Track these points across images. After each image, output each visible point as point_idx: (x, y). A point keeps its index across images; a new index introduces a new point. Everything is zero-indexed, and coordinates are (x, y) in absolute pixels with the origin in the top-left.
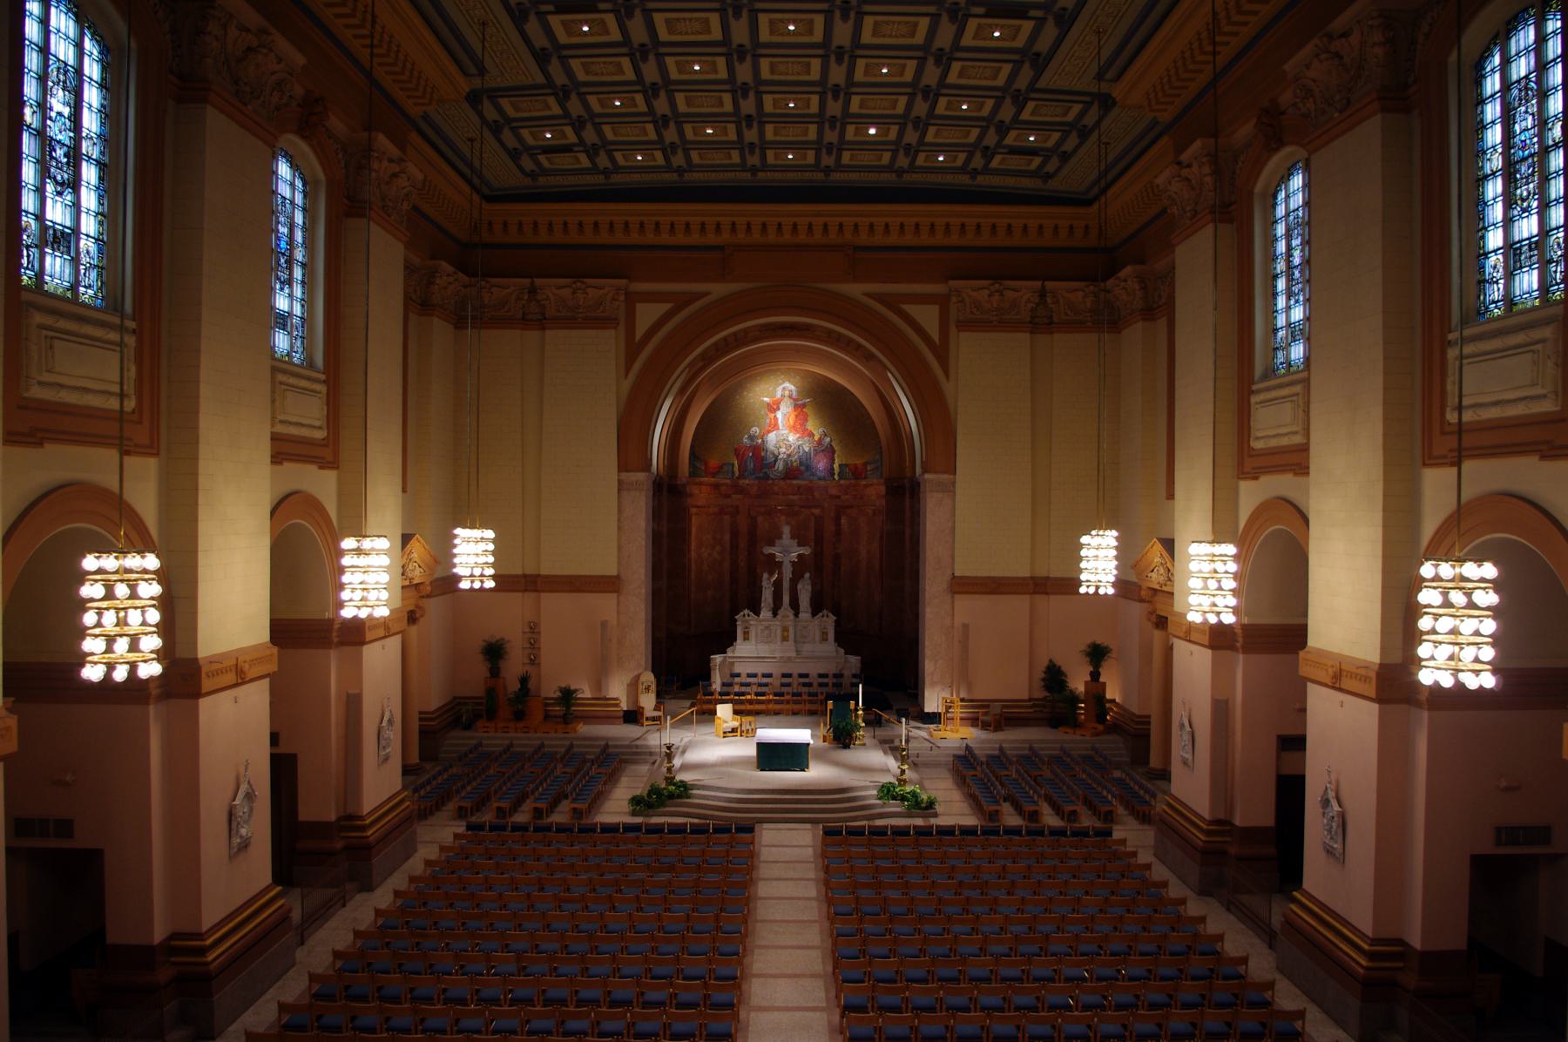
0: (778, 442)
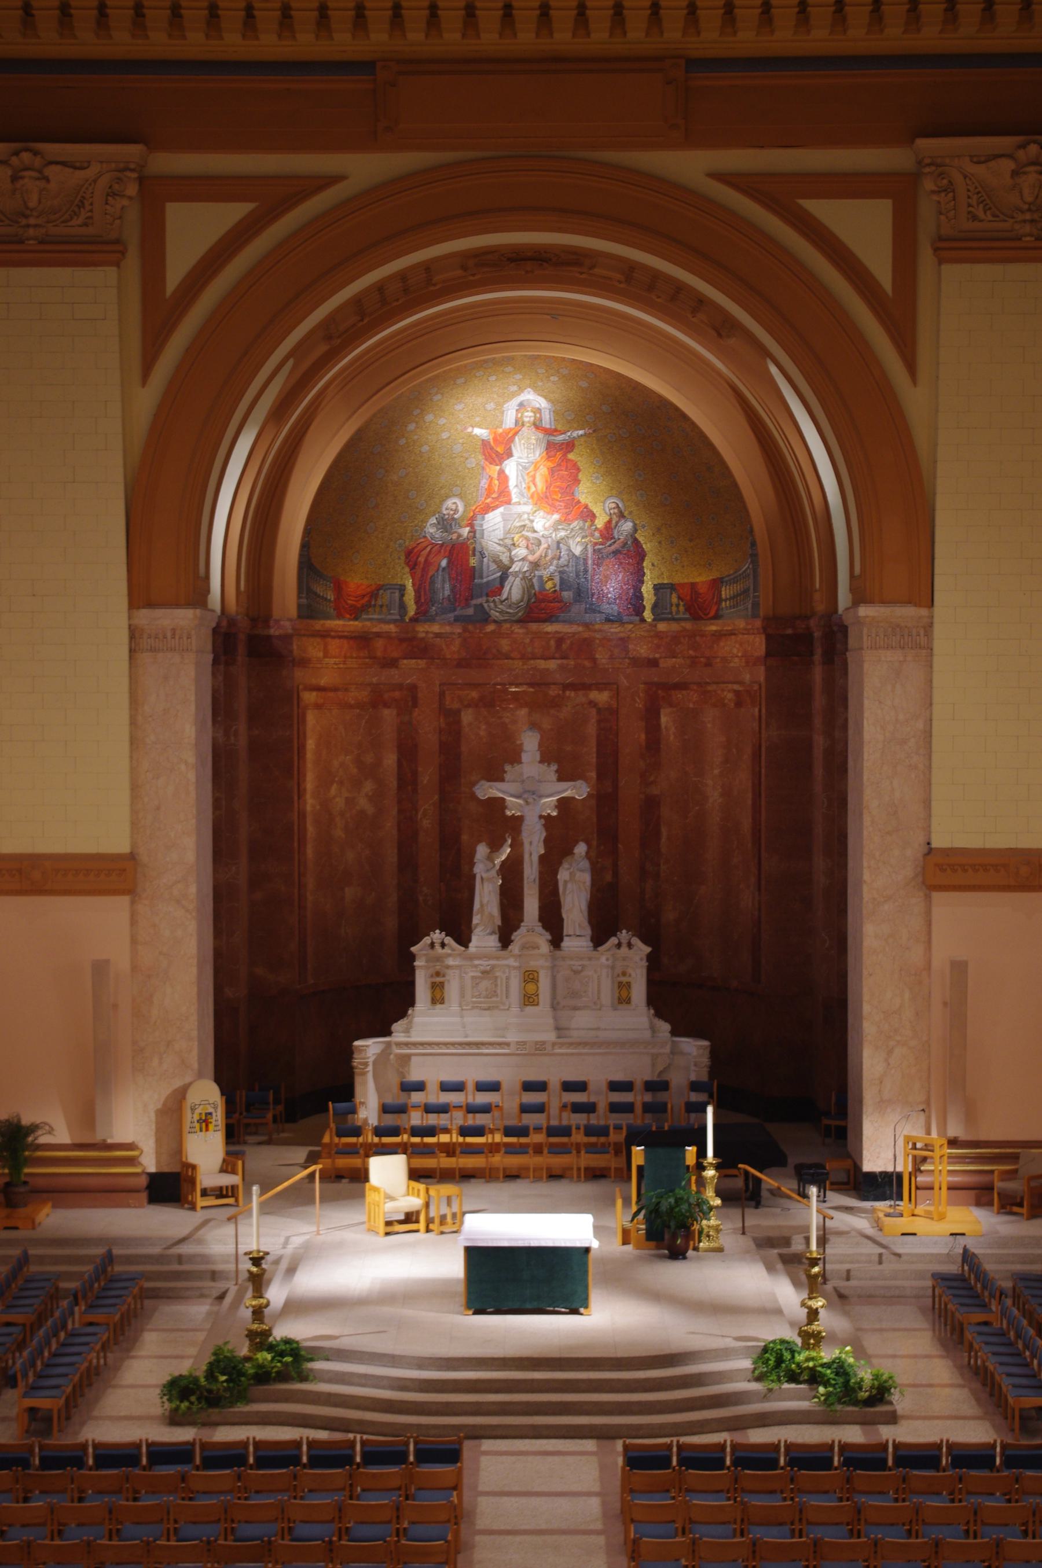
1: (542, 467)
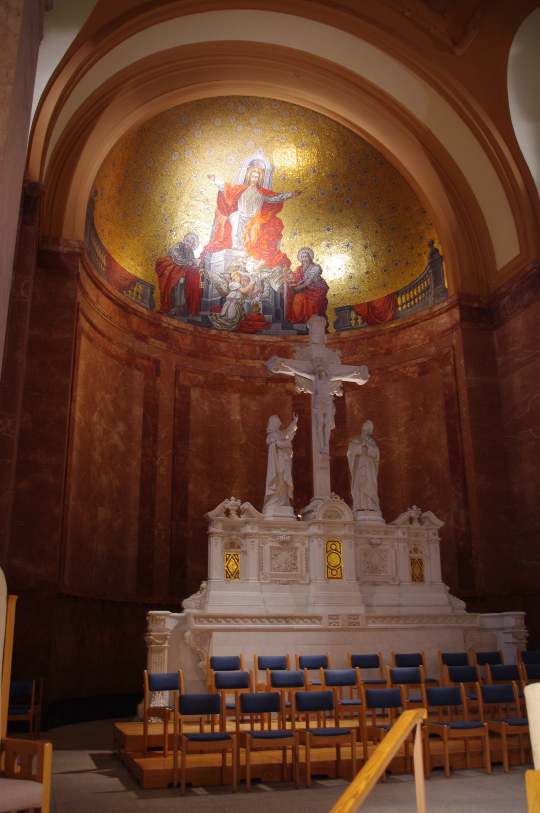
0: (228, 269)
1: (256, 222)
